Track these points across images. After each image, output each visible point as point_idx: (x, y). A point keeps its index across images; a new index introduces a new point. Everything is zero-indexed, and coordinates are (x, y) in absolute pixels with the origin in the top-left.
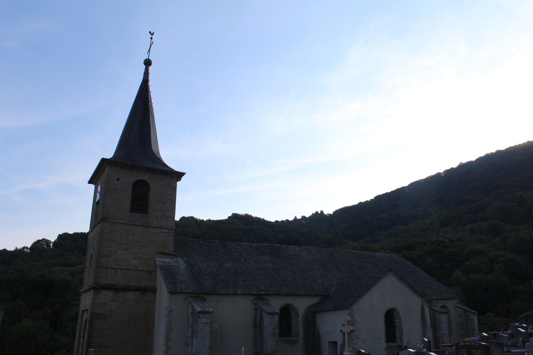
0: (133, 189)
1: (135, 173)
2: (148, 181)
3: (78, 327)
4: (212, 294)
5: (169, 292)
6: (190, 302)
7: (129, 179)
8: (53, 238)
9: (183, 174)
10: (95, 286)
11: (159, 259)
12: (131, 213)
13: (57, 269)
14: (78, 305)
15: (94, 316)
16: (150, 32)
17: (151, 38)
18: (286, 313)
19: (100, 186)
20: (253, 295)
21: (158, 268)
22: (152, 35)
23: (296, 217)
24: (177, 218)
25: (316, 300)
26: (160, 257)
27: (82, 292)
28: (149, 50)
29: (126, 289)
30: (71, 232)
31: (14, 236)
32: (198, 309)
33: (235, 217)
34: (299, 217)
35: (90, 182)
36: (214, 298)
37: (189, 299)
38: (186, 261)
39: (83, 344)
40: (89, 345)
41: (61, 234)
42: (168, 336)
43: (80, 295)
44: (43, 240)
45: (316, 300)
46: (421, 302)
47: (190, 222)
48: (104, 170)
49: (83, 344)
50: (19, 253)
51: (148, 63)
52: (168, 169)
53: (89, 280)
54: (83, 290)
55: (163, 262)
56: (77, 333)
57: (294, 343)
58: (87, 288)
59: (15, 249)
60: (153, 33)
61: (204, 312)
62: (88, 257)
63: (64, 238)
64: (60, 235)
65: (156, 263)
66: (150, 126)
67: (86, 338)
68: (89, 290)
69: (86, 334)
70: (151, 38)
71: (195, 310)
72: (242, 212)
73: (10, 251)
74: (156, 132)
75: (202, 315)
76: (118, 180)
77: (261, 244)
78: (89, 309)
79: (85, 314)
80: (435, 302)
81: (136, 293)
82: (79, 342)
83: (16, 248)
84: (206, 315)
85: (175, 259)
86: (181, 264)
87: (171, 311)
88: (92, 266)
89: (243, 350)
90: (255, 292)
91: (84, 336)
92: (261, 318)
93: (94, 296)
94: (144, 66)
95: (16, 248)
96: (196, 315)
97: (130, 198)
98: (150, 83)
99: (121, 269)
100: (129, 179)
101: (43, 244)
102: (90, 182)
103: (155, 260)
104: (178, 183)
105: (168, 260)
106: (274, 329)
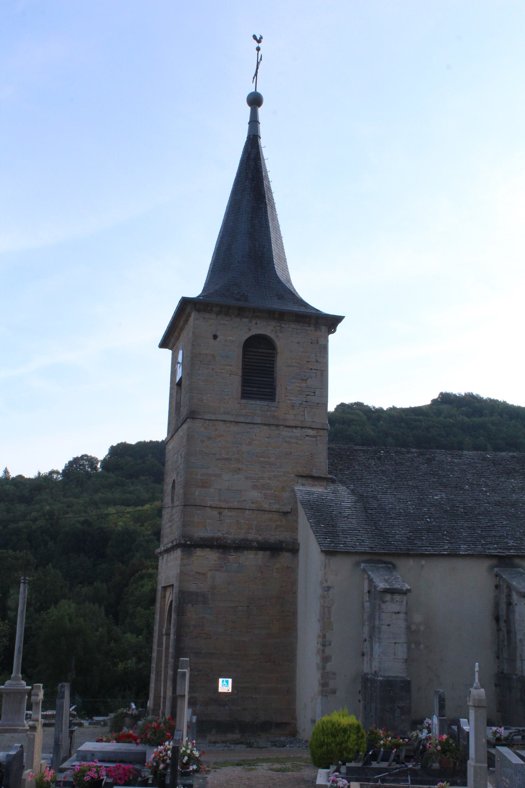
0: (244, 354)
1: (248, 318)
2: (272, 336)
3: (157, 617)
4: (407, 555)
5: (322, 551)
6: (364, 571)
7: (234, 334)
8: (100, 453)
9: (338, 319)
10: (183, 542)
11: (301, 488)
12: (244, 401)
13: (112, 510)
14: (153, 577)
15: (185, 598)
16: (255, 37)
17: (258, 49)
19: (181, 352)
21: (299, 505)
22: (259, 41)
24: (331, 407)
26: (303, 485)
27: (161, 553)
28: (256, 75)
29: (242, 546)
30: (133, 441)
31: (33, 447)
32: (382, 585)
33: (446, 399)
35: (164, 344)
36: (411, 562)
37: (363, 565)
38: (352, 491)
39: (167, 648)
40: (179, 652)
41: (115, 444)
42: (324, 636)
43: (157, 559)
47: (355, 416)
48: (187, 321)
49: (167, 648)
50: (44, 482)
51: (255, 101)
52: (309, 311)
53: (171, 530)
54: (162, 548)
55: (309, 493)
56: (156, 628)
58: (170, 545)
59: (37, 475)
60: (261, 38)
61: (392, 591)
62: (168, 488)
63: (120, 451)
64: (112, 447)
65: (295, 495)
66: (268, 227)
67: (172, 636)
68: (173, 548)
69: (172, 631)
70: (258, 49)
71: (375, 587)
72: (459, 388)
73: (29, 479)
74: (280, 238)
75: (388, 597)
76: (215, 337)
77: (503, 454)
78: (176, 584)
79: (168, 594)
81: (261, 553)
82: (160, 644)
83: (39, 473)
84: (397, 597)
85: (332, 487)
86: (343, 496)
87: (329, 588)
88: (176, 503)
89: (477, 669)
90: (493, 552)
91: (168, 635)
92: (509, 604)
93: (182, 559)
94: (249, 109)
95: (39, 473)
96: (378, 596)
97: (240, 372)
98: (263, 142)
99: (229, 509)
100: (234, 334)
101: (83, 465)
102: (164, 344)
103: (293, 491)
104: (331, 338)
105: (318, 489)
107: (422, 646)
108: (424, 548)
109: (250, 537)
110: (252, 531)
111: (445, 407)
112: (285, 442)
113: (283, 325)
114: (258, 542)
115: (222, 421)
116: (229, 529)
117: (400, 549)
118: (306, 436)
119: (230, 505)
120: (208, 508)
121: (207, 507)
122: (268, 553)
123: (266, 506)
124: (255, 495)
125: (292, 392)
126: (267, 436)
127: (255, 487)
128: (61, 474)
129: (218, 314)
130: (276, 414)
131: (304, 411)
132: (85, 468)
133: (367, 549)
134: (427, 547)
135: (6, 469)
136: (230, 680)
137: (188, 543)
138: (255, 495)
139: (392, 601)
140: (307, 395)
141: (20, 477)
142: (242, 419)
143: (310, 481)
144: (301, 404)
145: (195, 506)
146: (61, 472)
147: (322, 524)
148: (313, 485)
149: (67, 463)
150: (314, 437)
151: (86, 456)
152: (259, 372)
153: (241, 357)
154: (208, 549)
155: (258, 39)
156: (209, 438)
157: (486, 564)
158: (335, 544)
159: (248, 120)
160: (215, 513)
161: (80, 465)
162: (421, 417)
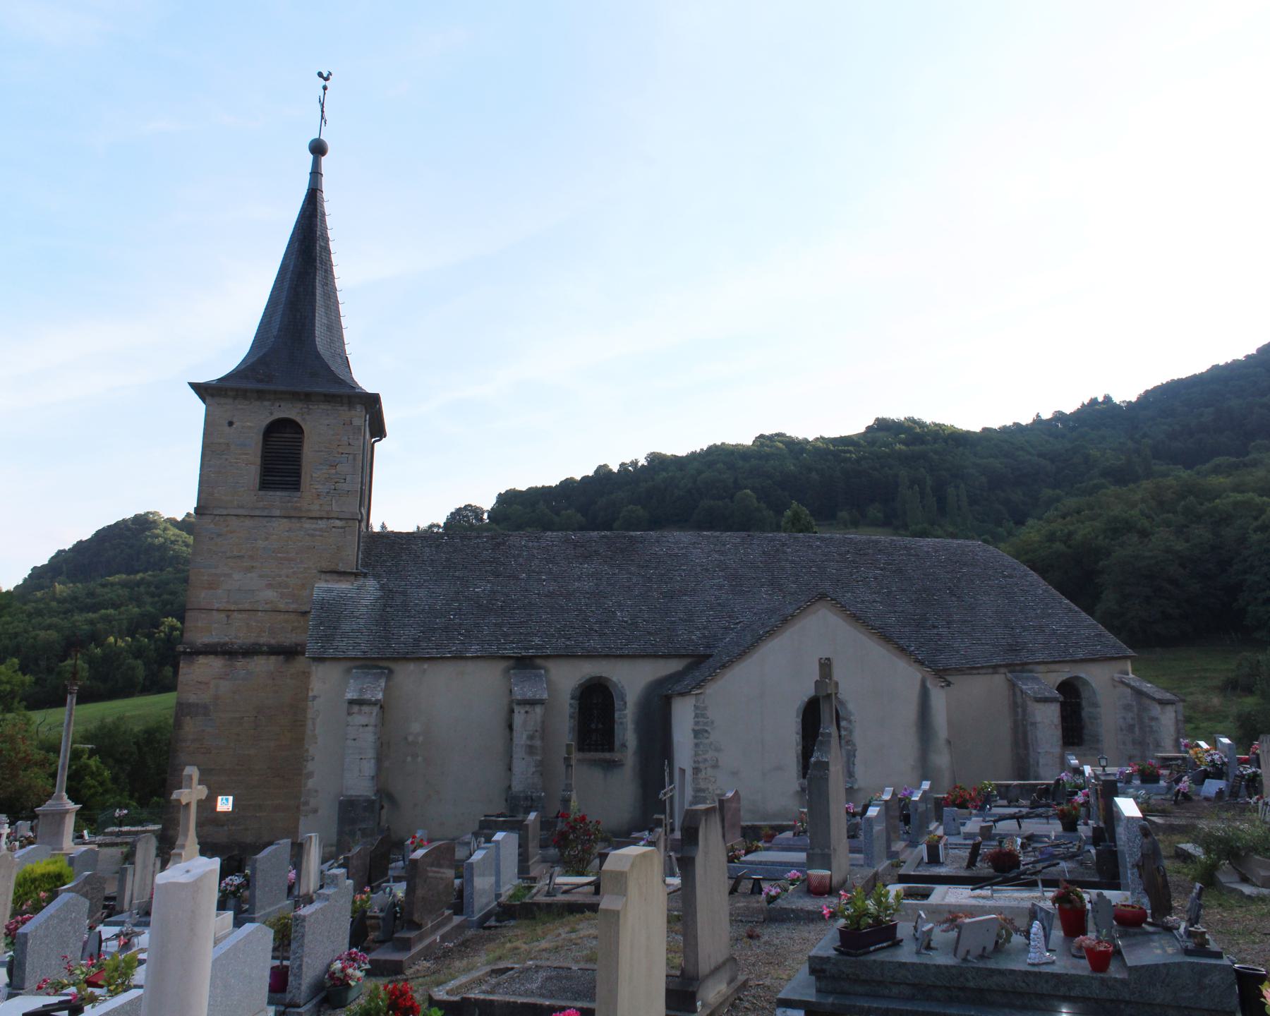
1: (291, 399)
2: (298, 419)
4: (405, 659)
8: (487, 502)
12: (261, 493)
16: (320, 75)
17: (325, 88)
18: (595, 702)
20: (504, 658)
22: (326, 79)
23: (1038, 416)
25: (674, 666)
26: (326, 581)
29: (250, 652)
30: (523, 487)
33: (883, 427)
34: (1047, 415)
36: (412, 667)
45: (674, 666)
46: (919, 676)
51: (318, 149)
55: (330, 590)
57: (611, 765)
60: (330, 74)
63: (509, 500)
70: (325, 88)
72: (897, 412)
75: (356, 708)
76: (231, 424)
80: (1041, 668)
81: (273, 658)
84: (366, 709)
85: (361, 581)
97: (258, 461)
99: (240, 611)
105: (344, 586)
106: (531, 737)
107: (420, 759)
109: (262, 640)
111: (881, 434)
114: (269, 646)
116: (239, 632)
119: (241, 607)
122: (281, 657)
123: (282, 606)
124: (270, 594)
127: (269, 586)
129: (235, 398)
136: (231, 798)
138: (270, 594)
139: (360, 712)
142: (257, 513)
143: (335, 577)
148: (338, 582)
152: (281, 461)
153: (260, 445)
156: (219, 535)
157: (503, 665)
159: (310, 170)
160: (223, 616)
162: (851, 448)
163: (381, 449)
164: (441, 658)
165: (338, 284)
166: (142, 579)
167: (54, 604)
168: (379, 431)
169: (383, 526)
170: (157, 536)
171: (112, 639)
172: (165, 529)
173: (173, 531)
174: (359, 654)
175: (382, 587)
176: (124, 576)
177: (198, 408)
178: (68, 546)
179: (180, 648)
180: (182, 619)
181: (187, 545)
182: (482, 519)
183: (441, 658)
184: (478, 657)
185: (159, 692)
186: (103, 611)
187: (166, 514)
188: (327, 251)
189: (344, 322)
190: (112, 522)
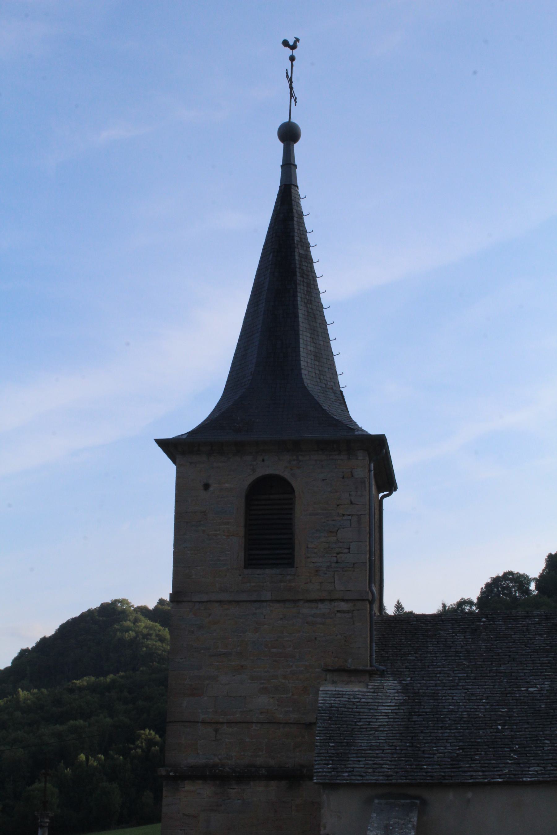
1: (280, 454)
2: (286, 475)
4: (441, 785)
7: (234, 479)
12: (246, 571)
16: (285, 43)
17: (292, 59)
22: (293, 47)
26: (334, 682)
29: (245, 775)
31: (2, 667)
36: (451, 795)
44: (508, 576)
51: (289, 134)
55: (338, 695)
59: (440, 608)
60: (297, 40)
70: (292, 59)
81: (274, 783)
83: (444, 606)
85: (376, 683)
94: (281, 146)
95: (444, 606)
97: (241, 531)
101: (508, 588)
105: (355, 688)
108: (469, 774)
110: (260, 753)
112: (307, 623)
113: (301, 458)
115: (217, 602)
117: (432, 776)
118: (338, 611)
120: (199, 724)
121: (198, 722)
125: (316, 550)
126: (281, 616)
128: (475, 605)
130: (293, 584)
131: (333, 577)
132: (511, 592)
133: (381, 778)
134: (475, 771)
135: (398, 602)
137: (171, 774)
140: (338, 553)
141: (411, 613)
144: (329, 567)
145: (182, 722)
146: (475, 601)
147: (332, 742)
148: (348, 683)
149: (483, 586)
150: (348, 612)
151: (510, 573)
154: (200, 782)
155: (291, 43)
158: (337, 772)
161: (504, 588)
163: (391, 505)
164: (489, 784)
165: (325, 299)
166: (113, 681)
167: (18, 714)
168: (388, 484)
169: (399, 607)
170: (127, 630)
171: (82, 757)
172: (136, 621)
173: (144, 623)
174: (381, 779)
175: (405, 689)
176: (93, 679)
177: (166, 471)
178: (30, 644)
179: (162, 771)
180: (161, 731)
181: (162, 639)
182: (527, 591)
183: (489, 784)
184: (539, 783)
185: (139, 824)
186: (72, 722)
187: (136, 602)
188: (309, 261)
189: (335, 347)
190: (76, 614)
